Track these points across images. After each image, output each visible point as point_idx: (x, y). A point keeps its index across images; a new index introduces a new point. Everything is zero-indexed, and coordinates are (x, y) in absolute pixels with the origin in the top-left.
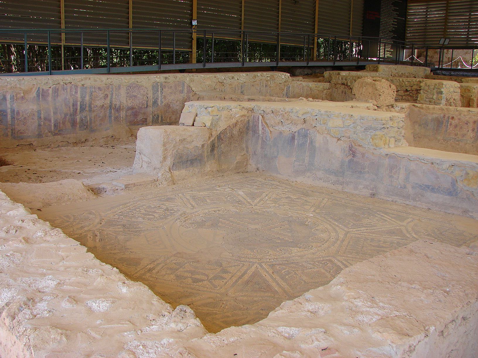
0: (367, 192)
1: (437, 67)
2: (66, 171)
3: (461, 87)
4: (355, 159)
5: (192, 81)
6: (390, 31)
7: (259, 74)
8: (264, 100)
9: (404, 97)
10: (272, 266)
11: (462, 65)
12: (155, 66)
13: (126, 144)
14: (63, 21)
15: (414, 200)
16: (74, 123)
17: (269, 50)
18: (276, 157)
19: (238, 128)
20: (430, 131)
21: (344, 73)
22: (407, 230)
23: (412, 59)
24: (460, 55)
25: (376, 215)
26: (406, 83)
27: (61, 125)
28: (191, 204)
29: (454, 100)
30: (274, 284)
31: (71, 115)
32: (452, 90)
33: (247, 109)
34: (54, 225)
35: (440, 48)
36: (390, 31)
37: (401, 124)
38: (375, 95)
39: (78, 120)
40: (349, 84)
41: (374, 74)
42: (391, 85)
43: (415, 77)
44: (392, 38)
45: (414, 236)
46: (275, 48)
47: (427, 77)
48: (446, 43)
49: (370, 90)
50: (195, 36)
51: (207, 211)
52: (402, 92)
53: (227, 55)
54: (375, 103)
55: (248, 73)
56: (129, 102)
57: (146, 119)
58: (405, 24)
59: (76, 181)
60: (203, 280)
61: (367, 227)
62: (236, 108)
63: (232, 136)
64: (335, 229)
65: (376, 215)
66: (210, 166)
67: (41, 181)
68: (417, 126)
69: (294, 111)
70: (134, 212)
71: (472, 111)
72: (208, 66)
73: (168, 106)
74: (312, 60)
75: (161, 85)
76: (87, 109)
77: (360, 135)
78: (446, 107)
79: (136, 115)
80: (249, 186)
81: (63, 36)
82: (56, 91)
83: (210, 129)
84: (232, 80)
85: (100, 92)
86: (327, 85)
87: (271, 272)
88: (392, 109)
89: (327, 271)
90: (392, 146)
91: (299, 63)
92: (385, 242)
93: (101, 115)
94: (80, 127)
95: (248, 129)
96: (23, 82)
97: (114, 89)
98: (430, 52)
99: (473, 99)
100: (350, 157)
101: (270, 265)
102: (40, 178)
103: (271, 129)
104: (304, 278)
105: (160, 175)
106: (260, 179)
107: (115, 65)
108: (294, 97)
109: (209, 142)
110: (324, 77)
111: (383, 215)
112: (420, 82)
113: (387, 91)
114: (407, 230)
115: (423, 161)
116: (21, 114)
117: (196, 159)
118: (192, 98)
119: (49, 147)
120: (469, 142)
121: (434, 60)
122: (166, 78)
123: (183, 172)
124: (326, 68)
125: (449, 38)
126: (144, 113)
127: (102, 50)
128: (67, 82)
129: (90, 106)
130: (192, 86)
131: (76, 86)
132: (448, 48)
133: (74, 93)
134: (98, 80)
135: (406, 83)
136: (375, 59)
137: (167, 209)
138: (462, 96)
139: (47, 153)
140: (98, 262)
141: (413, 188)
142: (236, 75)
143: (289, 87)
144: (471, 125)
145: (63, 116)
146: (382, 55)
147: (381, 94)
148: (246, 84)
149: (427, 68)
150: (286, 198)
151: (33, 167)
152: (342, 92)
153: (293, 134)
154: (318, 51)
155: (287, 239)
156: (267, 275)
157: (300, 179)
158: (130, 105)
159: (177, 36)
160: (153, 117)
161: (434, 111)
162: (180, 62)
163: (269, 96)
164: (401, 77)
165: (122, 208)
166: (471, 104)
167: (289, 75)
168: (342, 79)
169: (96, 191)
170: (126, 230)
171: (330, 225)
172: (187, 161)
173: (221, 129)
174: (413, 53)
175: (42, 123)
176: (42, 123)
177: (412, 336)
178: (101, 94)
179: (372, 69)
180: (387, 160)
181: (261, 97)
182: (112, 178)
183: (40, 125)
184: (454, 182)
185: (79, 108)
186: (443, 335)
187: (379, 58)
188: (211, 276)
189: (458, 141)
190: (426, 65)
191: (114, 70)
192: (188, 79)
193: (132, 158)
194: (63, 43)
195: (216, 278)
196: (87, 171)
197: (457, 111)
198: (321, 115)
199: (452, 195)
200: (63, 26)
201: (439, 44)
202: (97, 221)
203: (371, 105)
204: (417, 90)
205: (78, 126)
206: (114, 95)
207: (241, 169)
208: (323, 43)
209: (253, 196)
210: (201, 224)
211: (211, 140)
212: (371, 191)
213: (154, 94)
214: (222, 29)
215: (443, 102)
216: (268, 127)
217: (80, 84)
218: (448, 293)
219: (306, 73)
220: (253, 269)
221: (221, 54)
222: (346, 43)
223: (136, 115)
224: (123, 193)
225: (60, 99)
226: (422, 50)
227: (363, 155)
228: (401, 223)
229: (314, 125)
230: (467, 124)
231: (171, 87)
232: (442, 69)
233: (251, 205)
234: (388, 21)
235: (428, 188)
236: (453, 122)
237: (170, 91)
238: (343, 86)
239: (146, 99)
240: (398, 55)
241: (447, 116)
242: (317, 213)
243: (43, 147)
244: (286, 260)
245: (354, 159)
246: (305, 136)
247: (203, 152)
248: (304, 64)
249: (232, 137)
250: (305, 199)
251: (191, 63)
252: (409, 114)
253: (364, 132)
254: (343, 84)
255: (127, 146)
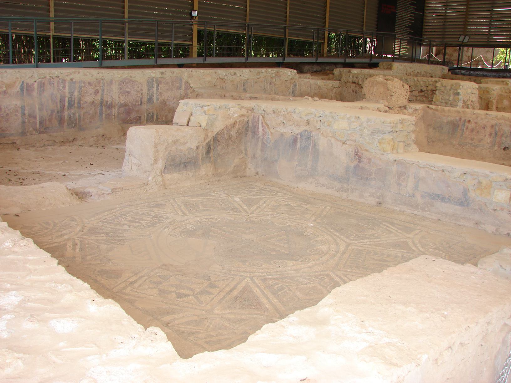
0: (372, 201)
1: (455, 65)
2: (50, 172)
3: (480, 88)
4: (361, 165)
5: (190, 76)
6: (406, 27)
7: (263, 70)
8: (267, 99)
9: (418, 98)
10: (265, 280)
11: (483, 65)
12: (151, 60)
13: (118, 144)
14: (52, 9)
15: (423, 210)
16: (61, 121)
17: (274, 44)
18: (277, 161)
19: (236, 129)
20: (443, 137)
21: (355, 71)
22: (413, 243)
23: (430, 56)
24: (480, 54)
25: (382, 226)
26: (422, 83)
27: (48, 123)
28: (182, 211)
29: (472, 102)
30: (264, 301)
31: (58, 112)
32: (469, 91)
33: (246, 108)
34: (25, 234)
35: (460, 46)
36: (406, 27)
37: (412, 128)
38: (387, 95)
39: (66, 117)
40: (360, 83)
41: (387, 72)
42: (404, 84)
43: (432, 77)
44: (409, 34)
45: (421, 249)
46: (281, 42)
47: (444, 77)
48: (466, 40)
49: (382, 90)
50: (196, 28)
51: (198, 219)
52: (417, 92)
53: (231, 50)
54: (387, 104)
55: (252, 69)
56: (122, 98)
57: (140, 117)
58: (423, 19)
59: (58, 184)
60: (188, 295)
61: (370, 239)
62: (234, 107)
63: (230, 138)
64: (335, 241)
65: (382, 226)
66: (205, 170)
67: (21, 184)
68: (431, 130)
69: (297, 111)
70: (120, 218)
71: (489, 115)
72: (209, 60)
73: (164, 103)
74: (322, 56)
75: (157, 80)
76: (76, 105)
77: (367, 138)
78: (463, 110)
79: (128, 112)
80: (246, 192)
81: (52, 25)
82: (42, 86)
83: (206, 130)
84: (234, 77)
85: (90, 87)
86: (336, 83)
87: (263, 287)
88: (405, 111)
89: (323, 287)
90: (401, 151)
91: (307, 59)
92: (389, 256)
93: (91, 112)
94: (68, 125)
95: (247, 130)
96: (5, 75)
97: (106, 84)
98: (449, 50)
99: (492, 102)
100: (356, 162)
101: (262, 280)
102: (21, 181)
103: (272, 131)
104: (299, 294)
105: (150, 178)
106: (259, 184)
107: (110, 58)
108: (301, 95)
109: (204, 144)
110: (333, 74)
111: (388, 225)
112: (436, 82)
113: (399, 90)
114: (413, 243)
115: (433, 168)
116: (3, 110)
117: (190, 162)
118: (190, 95)
119: (33, 146)
120: (485, 147)
121: (453, 58)
122: (162, 73)
123: (176, 175)
124: (336, 65)
125: (469, 36)
126: (138, 111)
127: (95, 41)
128: (54, 76)
129: (79, 103)
130: (190, 82)
131: (64, 81)
132: (468, 46)
133: (61, 88)
134: (88, 74)
135: (422, 83)
136: (390, 56)
137: (156, 216)
138: (480, 98)
139: (31, 153)
140: (68, 276)
141: (422, 196)
142: (238, 71)
143: (296, 85)
144: (488, 130)
145: (49, 112)
146: (397, 52)
147: (393, 94)
148: (249, 81)
149: (444, 67)
150: (286, 205)
151: (14, 168)
152: (353, 91)
153: (296, 137)
154: (329, 46)
155: (283, 251)
156: (258, 290)
157: (302, 185)
158: (122, 102)
159: (175, 27)
160: (148, 115)
161: (449, 113)
162: (181, 56)
163: (272, 93)
164: (416, 76)
165: (108, 215)
166: (490, 107)
167: (295, 71)
168: (353, 77)
169: (81, 195)
170: (110, 238)
171: (331, 236)
172: (180, 164)
173: (218, 130)
174: (430, 51)
175: (26, 120)
176: (26, 120)
177: (400, 366)
178: (91, 90)
179: (386, 67)
180: (395, 166)
181: (264, 96)
182: (98, 182)
183: (23, 122)
184: (465, 192)
185: (67, 104)
186: (437, 363)
187: (394, 55)
188: (197, 290)
189: (474, 146)
190: (443, 63)
191: (106, 63)
192: (186, 75)
193: (122, 159)
194: (52, 33)
195: (202, 293)
196: (72, 172)
197: (474, 114)
198: (326, 116)
199: (463, 206)
200: (52, 15)
201: (458, 41)
202: (79, 228)
203: (382, 106)
204: (433, 91)
205: (66, 124)
206: (105, 91)
207: (239, 174)
208: (334, 38)
209: (250, 203)
210: (191, 233)
211: (207, 141)
212: (377, 200)
213: (149, 90)
214: (225, 20)
215: (460, 104)
216: (269, 128)
217: (68, 79)
218: (445, 316)
219: (315, 70)
220: (244, 283)
221: (224, 48)
222: (359, 38)
223: (128, 112)
224: (109, 198)
225: (46, 94)
226: (441, 48)
227: (370, 160)
228: (408, 235)
229: (318, 127)
230: (484, 128)
231: (168, 83)
232: (461, 69)
233: (247, 213)
234: (404, 15)
235: (439, 197)
236: (470, 126)
237: (166, 87)
238: (354, 85)
239: (140, 96)
240: (414, 53)
241: (463, 119)
242: (317, 223)
243: (27, 146)
244: (280, 275)
245: (360, 167)
246: (308, 138)
247: (198, 154)
248: (313, 60)
249: (230, 139)
250: (306, 207)
251: (192, 57)
252: (423, 116)
253: (371, 135)
254: (354, 83)
255: (118, 146)
